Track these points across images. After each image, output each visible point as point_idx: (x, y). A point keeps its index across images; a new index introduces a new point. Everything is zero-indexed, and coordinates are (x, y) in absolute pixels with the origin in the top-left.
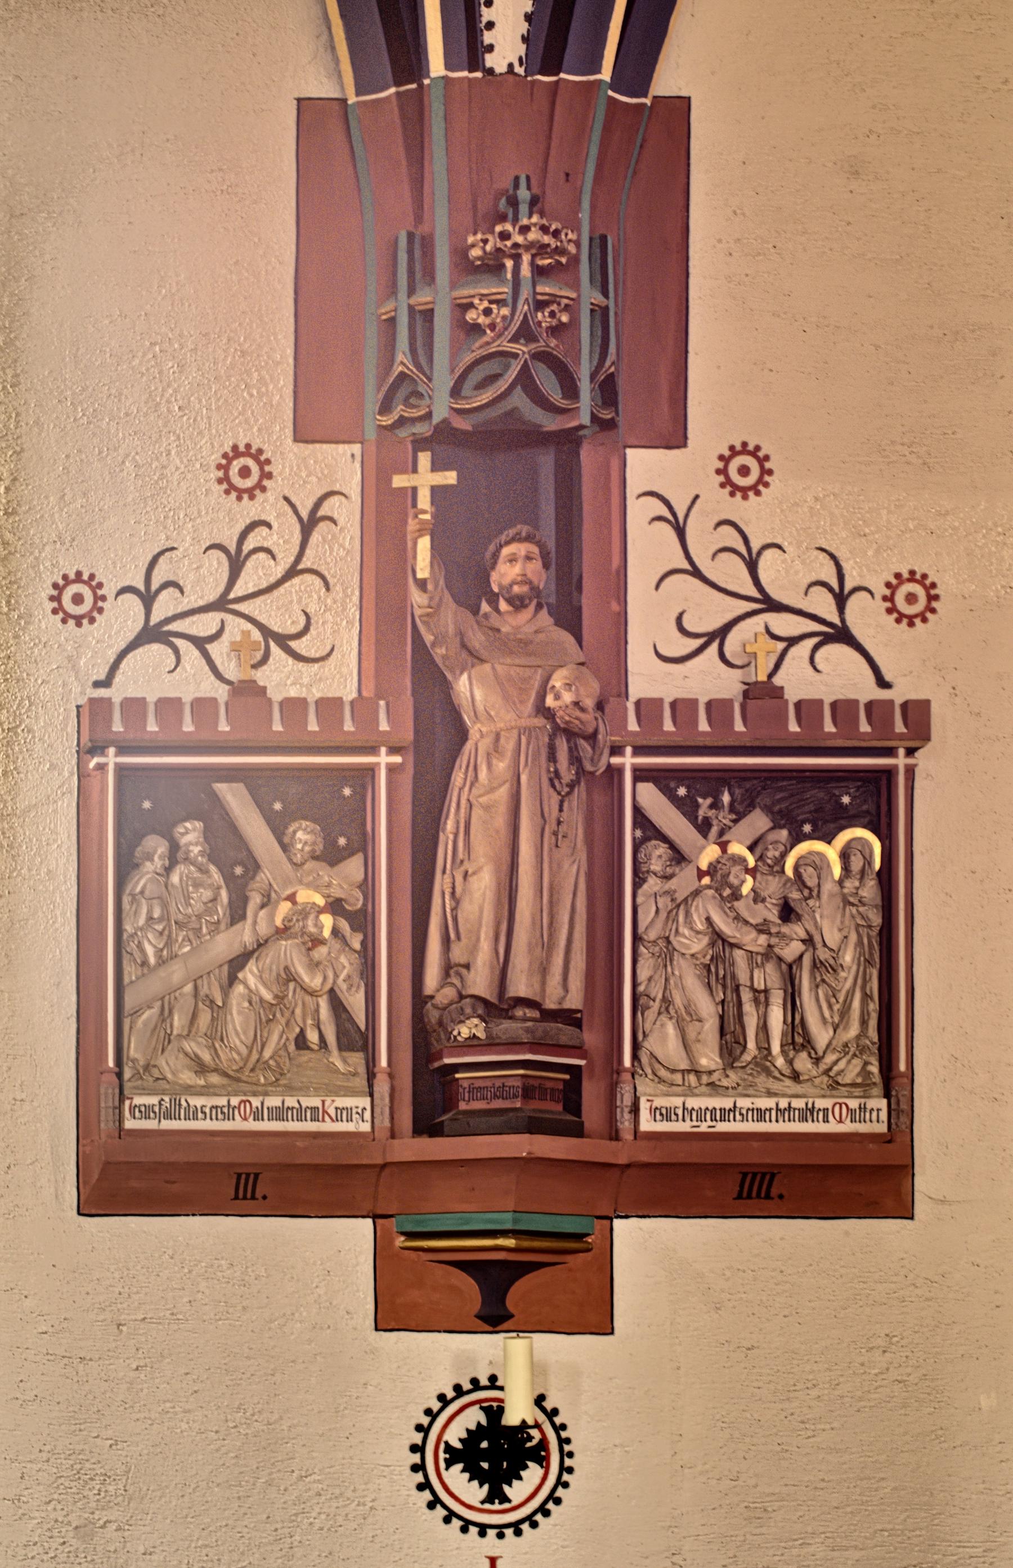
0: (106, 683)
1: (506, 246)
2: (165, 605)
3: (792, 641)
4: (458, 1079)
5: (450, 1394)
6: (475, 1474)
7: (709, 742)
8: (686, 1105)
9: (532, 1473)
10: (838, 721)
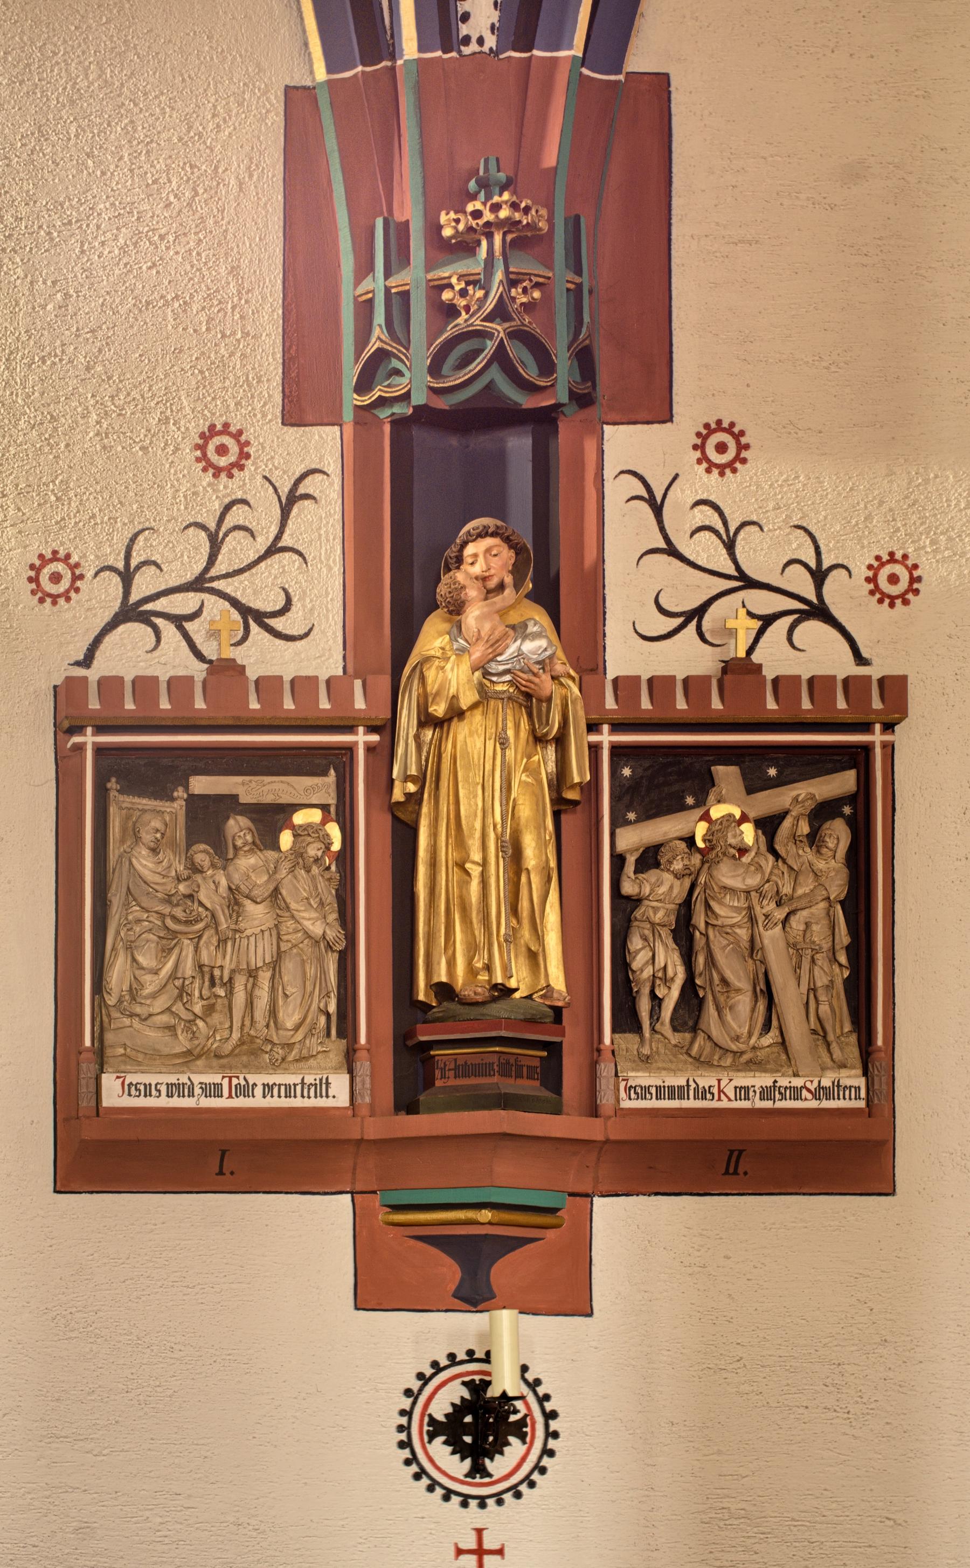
0: (87, 661)
1: (477, 224)
2: (143, 585)
3: (768, 621)
4: (434, 1056)
5: (428, 1371)
6: (460, 1449)
7: (810, 717)
8: (841, 1083)
9: (515, 1448)
10: (781, 696)
